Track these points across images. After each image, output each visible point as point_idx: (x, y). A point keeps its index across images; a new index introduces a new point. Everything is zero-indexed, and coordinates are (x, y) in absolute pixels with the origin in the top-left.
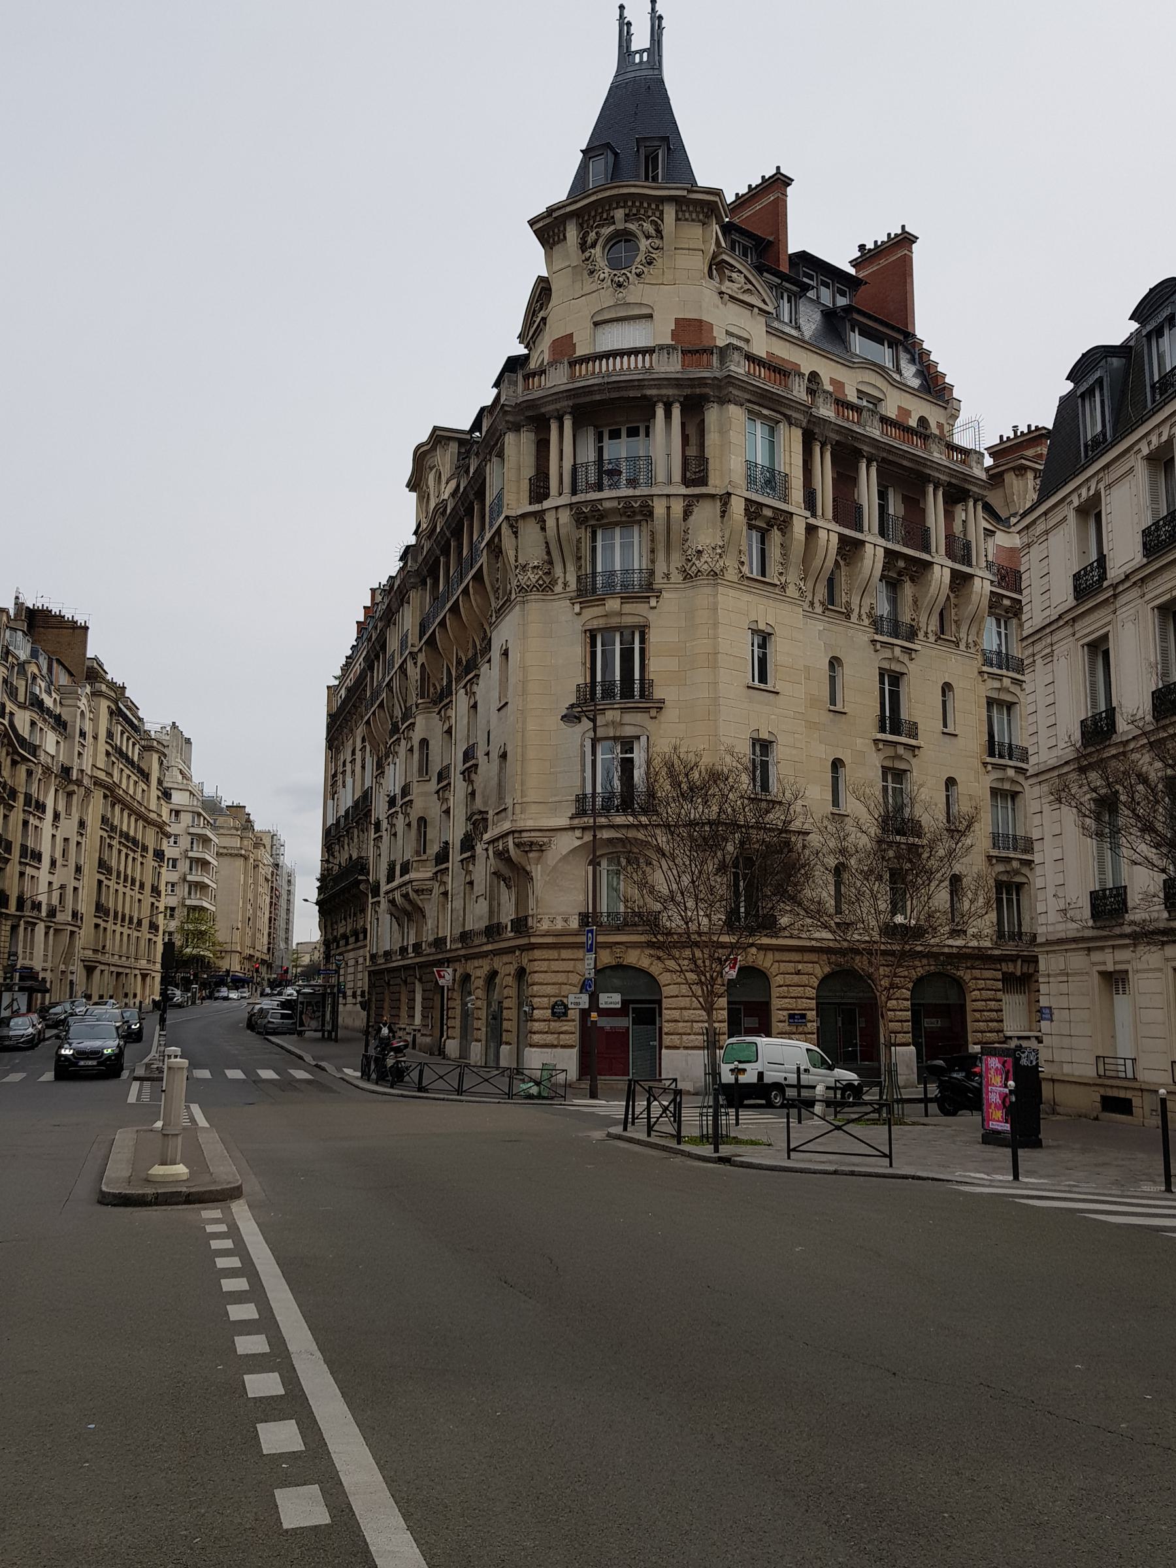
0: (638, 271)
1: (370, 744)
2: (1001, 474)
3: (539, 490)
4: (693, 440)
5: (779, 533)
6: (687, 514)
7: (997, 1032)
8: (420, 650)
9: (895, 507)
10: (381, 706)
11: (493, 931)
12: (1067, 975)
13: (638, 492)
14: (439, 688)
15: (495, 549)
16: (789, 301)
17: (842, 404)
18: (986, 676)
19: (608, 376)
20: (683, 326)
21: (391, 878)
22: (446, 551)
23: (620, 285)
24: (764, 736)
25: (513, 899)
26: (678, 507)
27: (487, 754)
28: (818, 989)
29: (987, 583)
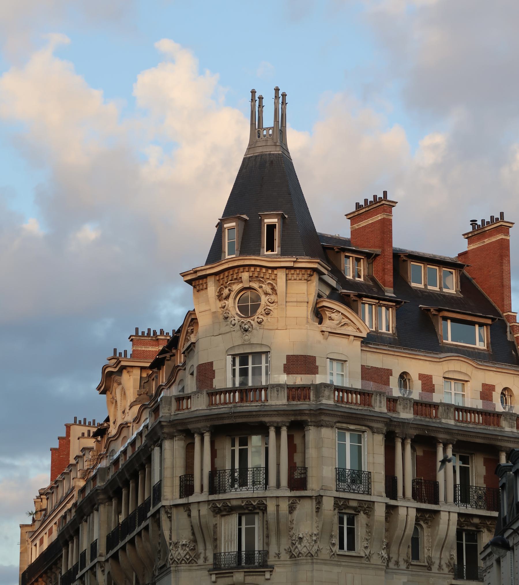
0: (259, 320)
3: (187, 488)
5: (365, 516)
6: (292, 509)
8: (107, 561)
19: (235, 407)
23: (246, 330)
26: (284, 506)
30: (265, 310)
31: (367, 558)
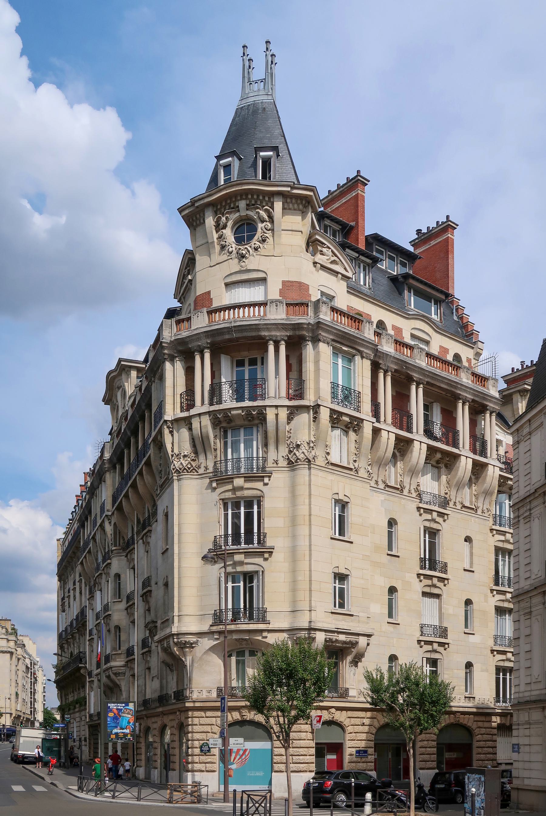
1: (85, 579)
2: (511, 395)
4: (295, 367)
6: (290, 419)
7: (492, 760)
8: (113, 514)
9: (437, 418)
10: (89, 552)
11: (162, 699)
12: (530, 724)
13: (255, 404)
14: (126, 540)
15: (160, 445)
16: (364, 270)
17: (399, 343)
18: (495, 532)
19: (235, 322)
20: (287, 285)
21: (98, 666)
22: (128, 446)
24: (342, 571)
25: (175, 680)
26: (283, 414)
27: (156, 584)
28: (438, 736)
29: (497, 469)
30: (261, 236)
31: (356, 470)
